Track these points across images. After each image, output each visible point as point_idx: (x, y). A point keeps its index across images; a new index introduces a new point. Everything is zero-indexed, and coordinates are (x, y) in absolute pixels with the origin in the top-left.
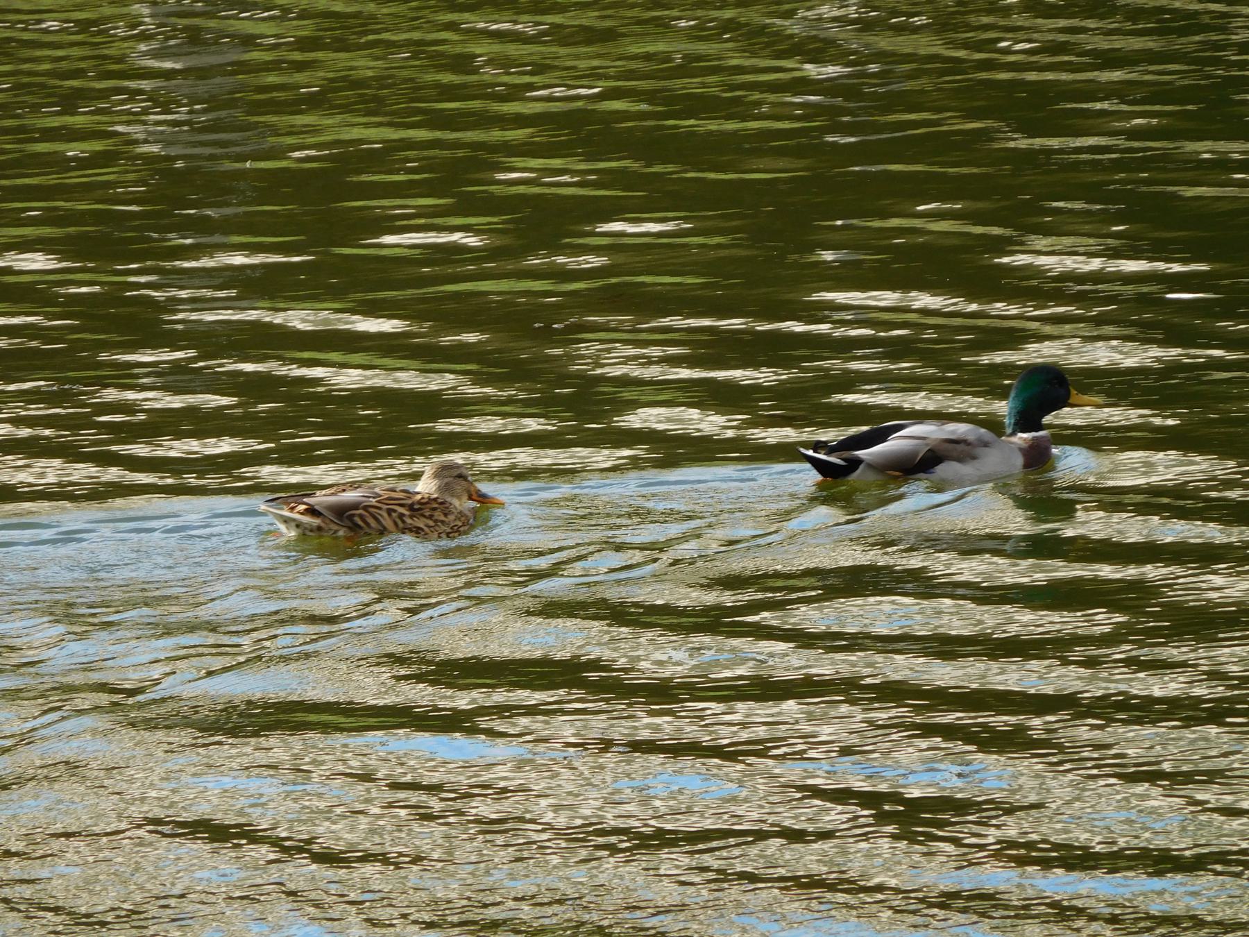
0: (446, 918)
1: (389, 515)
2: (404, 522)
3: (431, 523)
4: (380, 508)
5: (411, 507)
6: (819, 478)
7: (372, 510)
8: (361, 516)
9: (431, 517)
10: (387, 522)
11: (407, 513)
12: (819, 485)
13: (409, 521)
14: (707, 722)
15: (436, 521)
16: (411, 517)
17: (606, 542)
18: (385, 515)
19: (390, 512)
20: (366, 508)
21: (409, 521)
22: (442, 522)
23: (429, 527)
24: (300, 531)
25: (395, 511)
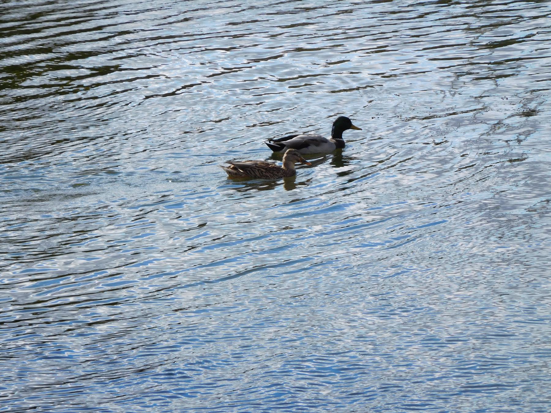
0: (424, 243)
1: (258, 171)
2: (262, 174)
3: (272, 175)
4: (256, 169)
5: (266, 169)
6: (272, 152)
7: (253, 169)
8: (249, 170)
9: (272, 173)
10: (257, 174)
11: (264, 171)
12: (273, 154)
13: (264, 173)
14: (180, 387)
15: (274, 174)
16: (265, 172)
17: (524, 191)
18: (257, 171)
19: (258, 170)
20: (251, 168)
21: (264, 173)
22: (276, 175)
23: (271, 176)
24: (283, 178)
25: (260, 170)
